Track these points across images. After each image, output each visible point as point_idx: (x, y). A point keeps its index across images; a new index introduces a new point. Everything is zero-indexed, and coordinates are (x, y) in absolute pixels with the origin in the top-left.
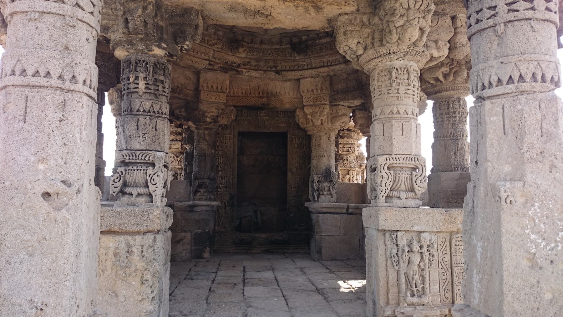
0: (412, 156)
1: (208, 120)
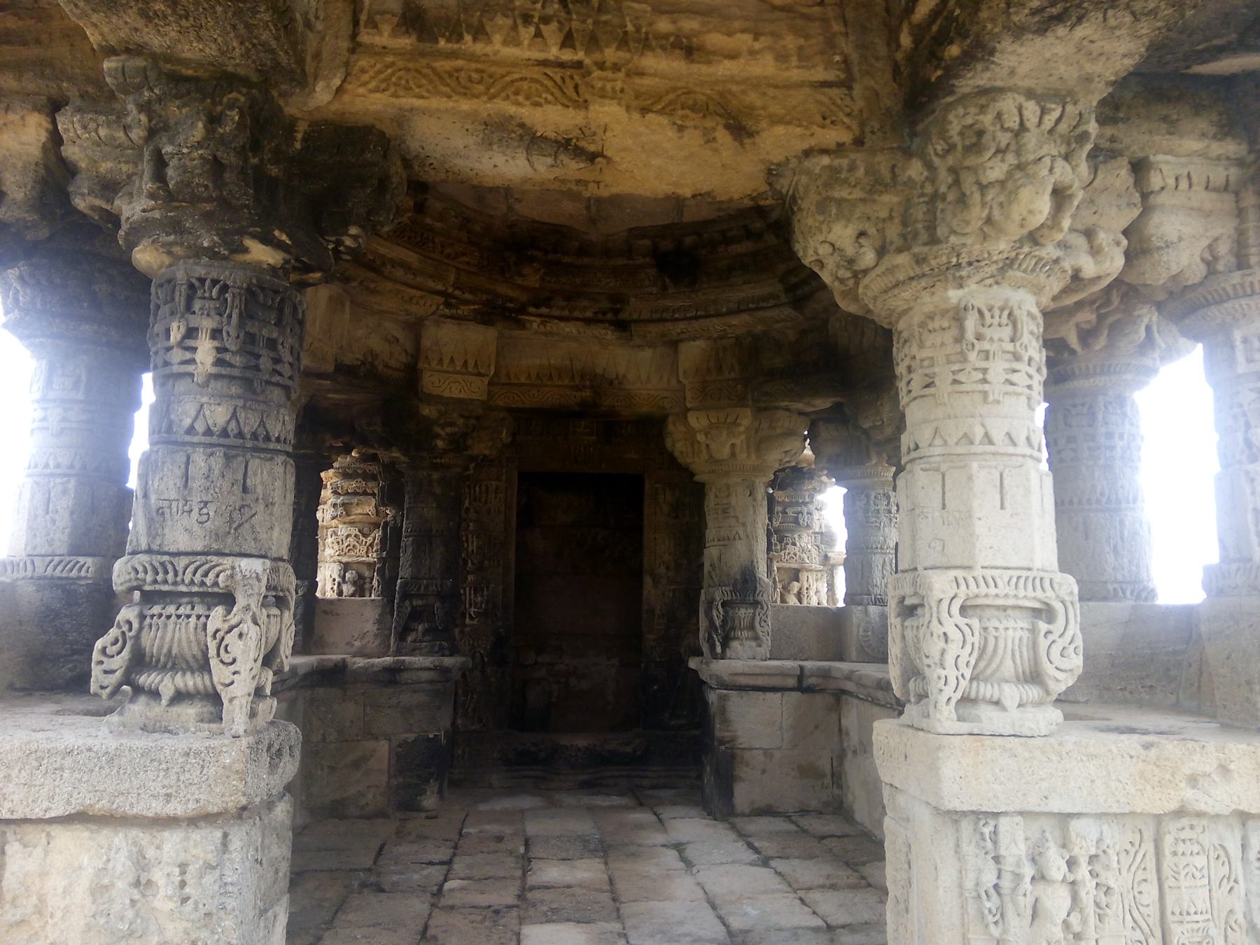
0: (1031, 574)
1: (440, 443)
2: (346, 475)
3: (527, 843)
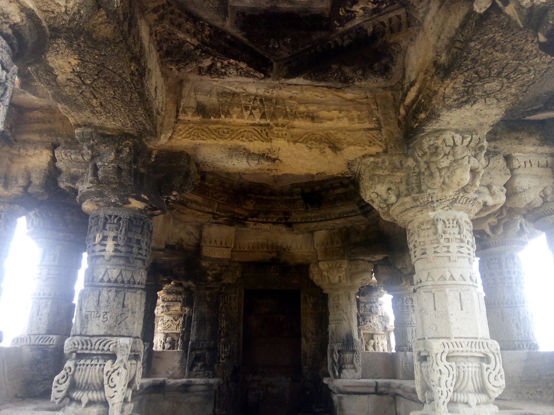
0: (478, 341)
1: (210, 278)
2: (168, 293)
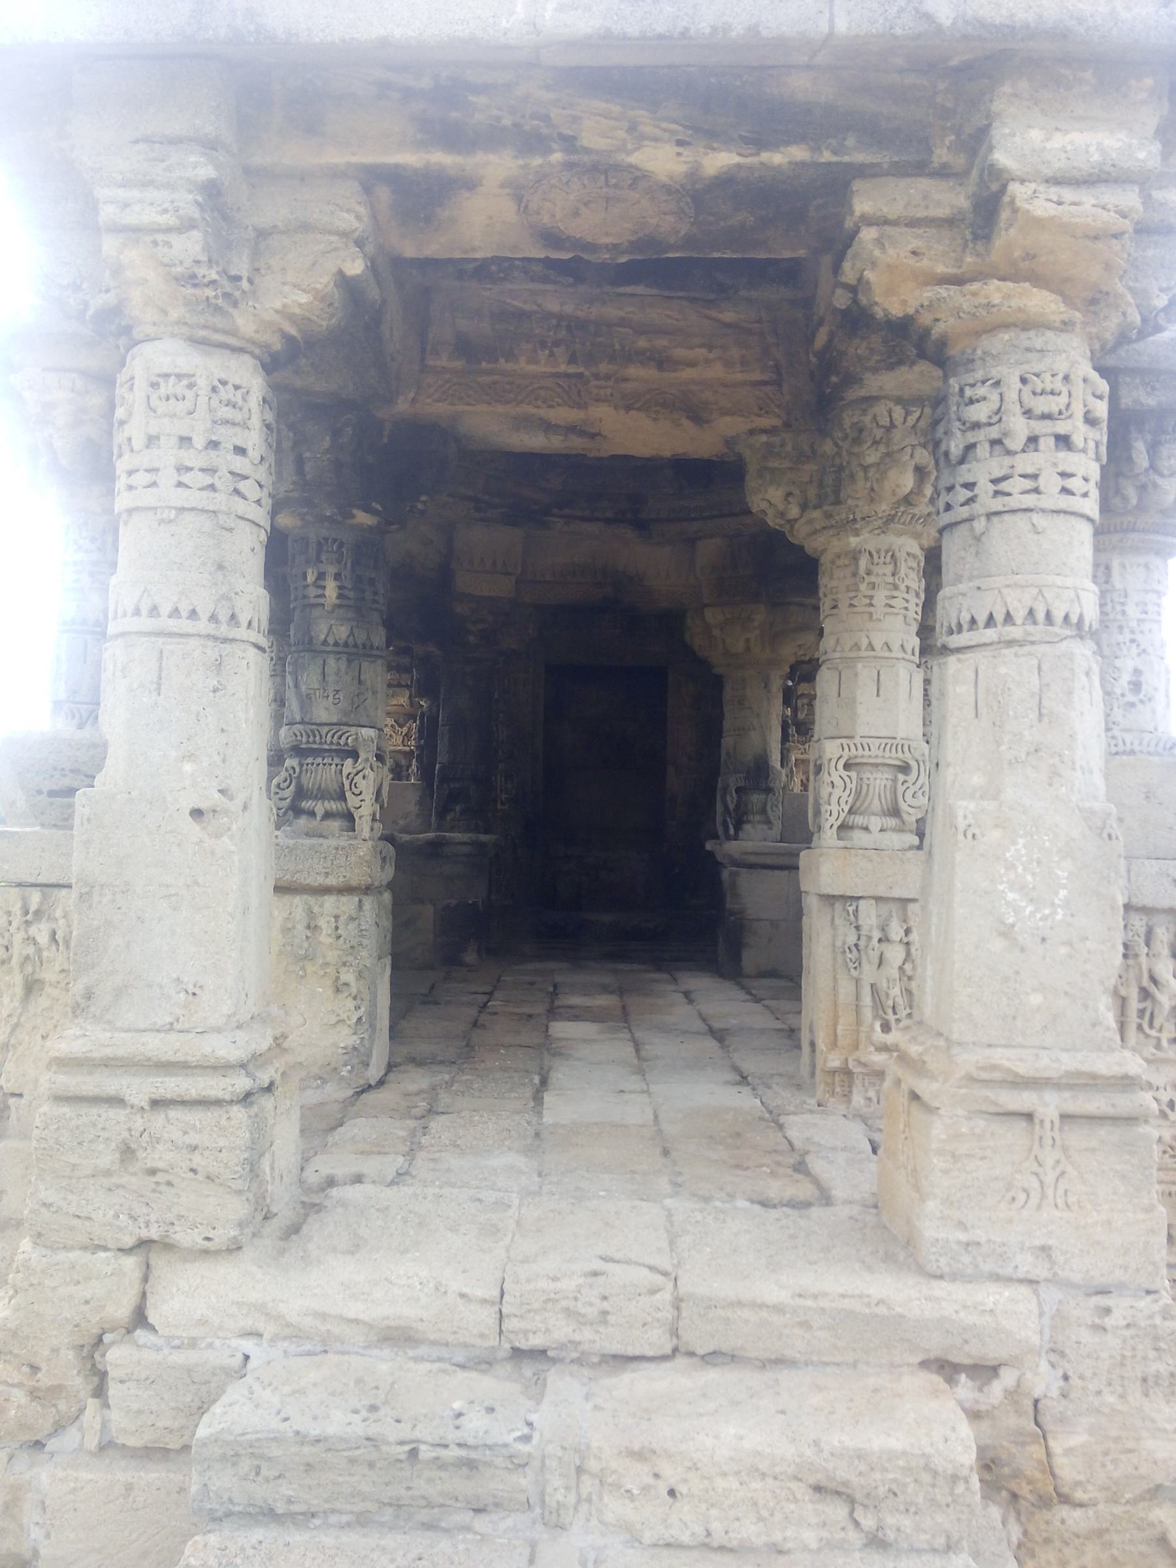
1: (472, 639)
3: (555, 987)
